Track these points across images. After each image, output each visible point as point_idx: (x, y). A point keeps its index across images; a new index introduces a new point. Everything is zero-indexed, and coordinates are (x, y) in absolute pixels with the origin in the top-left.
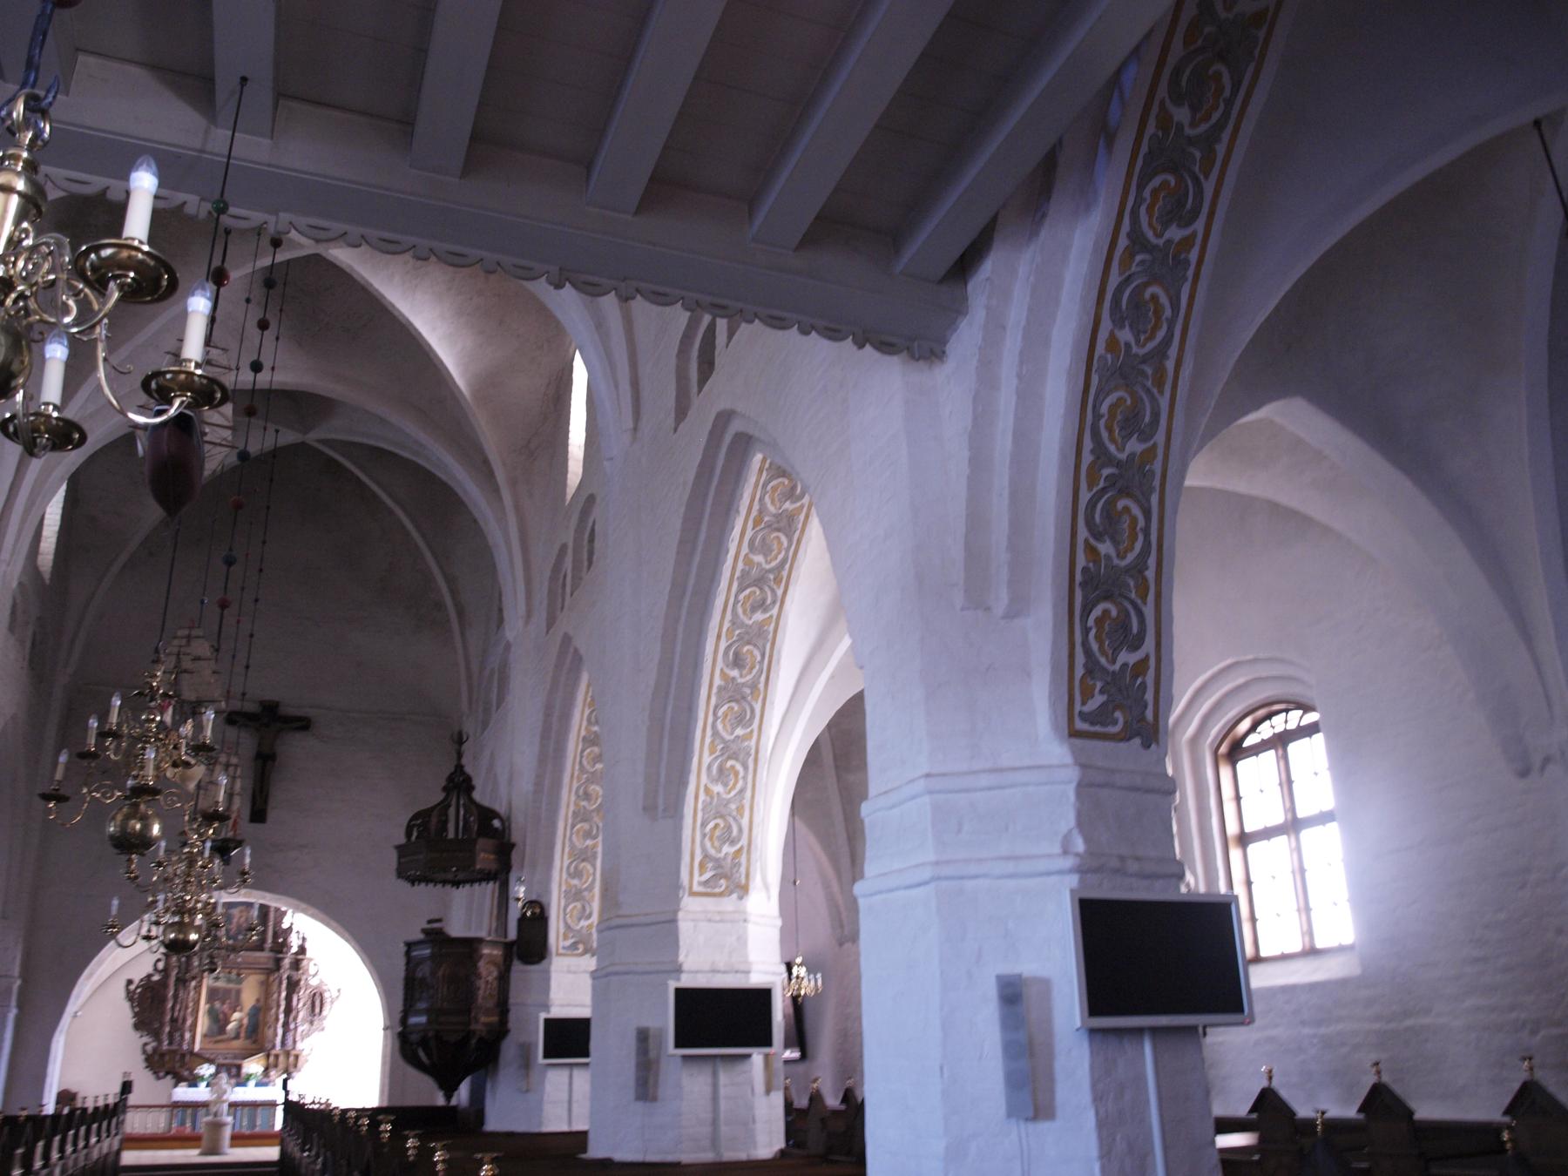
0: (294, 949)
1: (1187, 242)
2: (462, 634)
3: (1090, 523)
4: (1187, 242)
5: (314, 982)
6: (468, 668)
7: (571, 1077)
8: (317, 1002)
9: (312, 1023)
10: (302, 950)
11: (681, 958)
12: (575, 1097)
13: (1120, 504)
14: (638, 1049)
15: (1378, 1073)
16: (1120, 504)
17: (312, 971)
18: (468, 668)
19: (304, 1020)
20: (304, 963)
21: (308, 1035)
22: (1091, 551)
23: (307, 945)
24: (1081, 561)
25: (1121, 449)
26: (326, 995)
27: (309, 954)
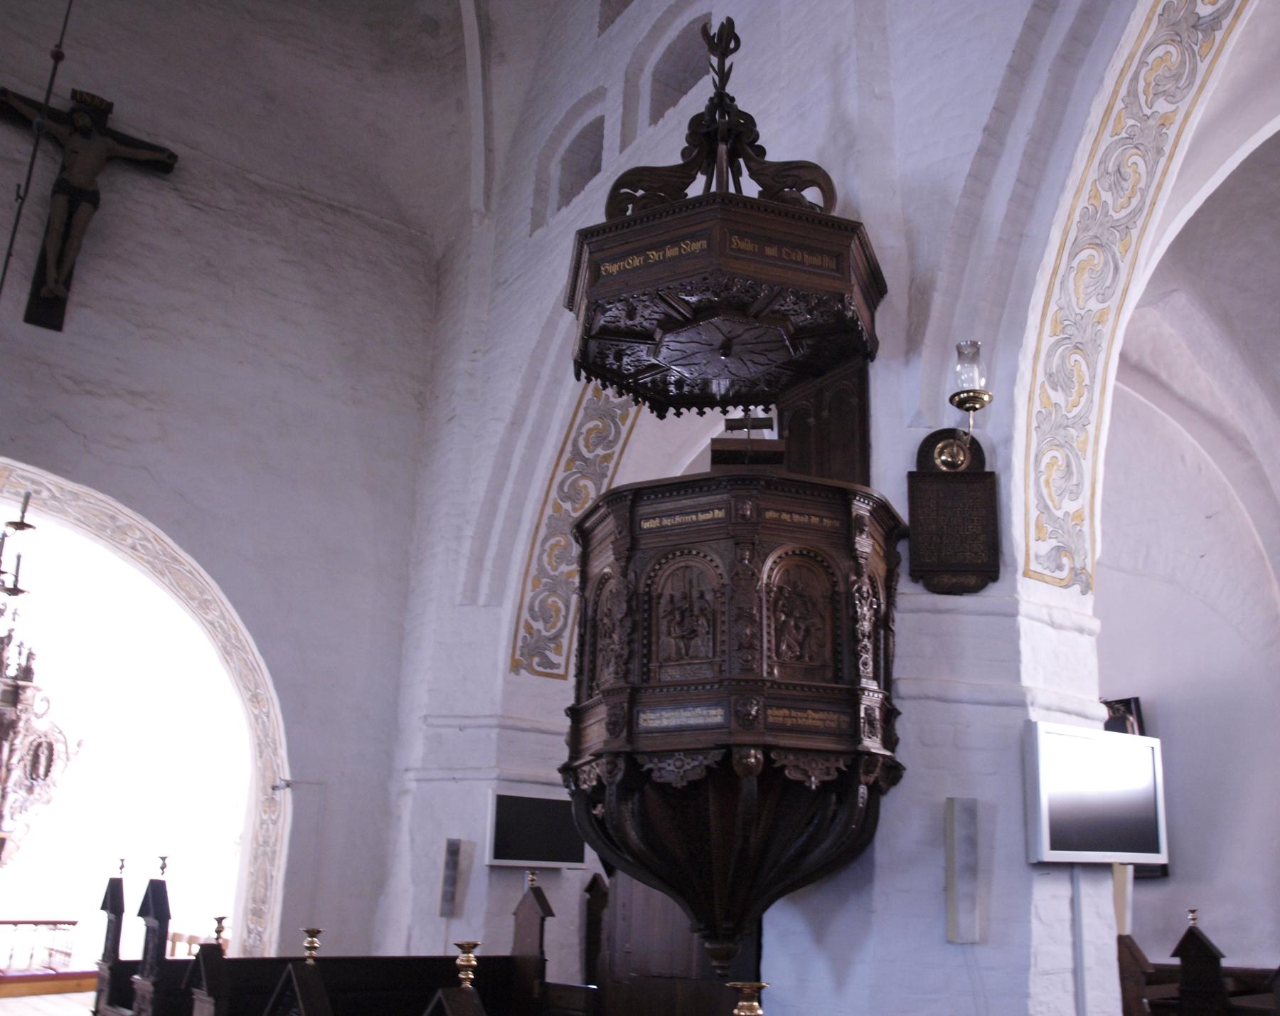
0: (12, 671)
1: (607, 458)
2: (485, 69)
3: (531, 609)
4: (607, 458)
5: (40, 725)
6: (488, 137)
7: (1074, 903)
8: (41, 760)
9: (30, 790)
10: (27, 673)
11: (1026, 680)
12: (1089, 960)
13: (550, 601)
14: (460, 886)
15: (219, 931)
16: (550, 601)
17: (39, 707)
18: (488, 137)
19: (19, 785)
20: (29, 693)
21: (23, 808)
22: (529, 628)
23: (35, 665)
24: (522, 632)
25: (555, 569)
26: (58, 748)
27: (37, 679)
